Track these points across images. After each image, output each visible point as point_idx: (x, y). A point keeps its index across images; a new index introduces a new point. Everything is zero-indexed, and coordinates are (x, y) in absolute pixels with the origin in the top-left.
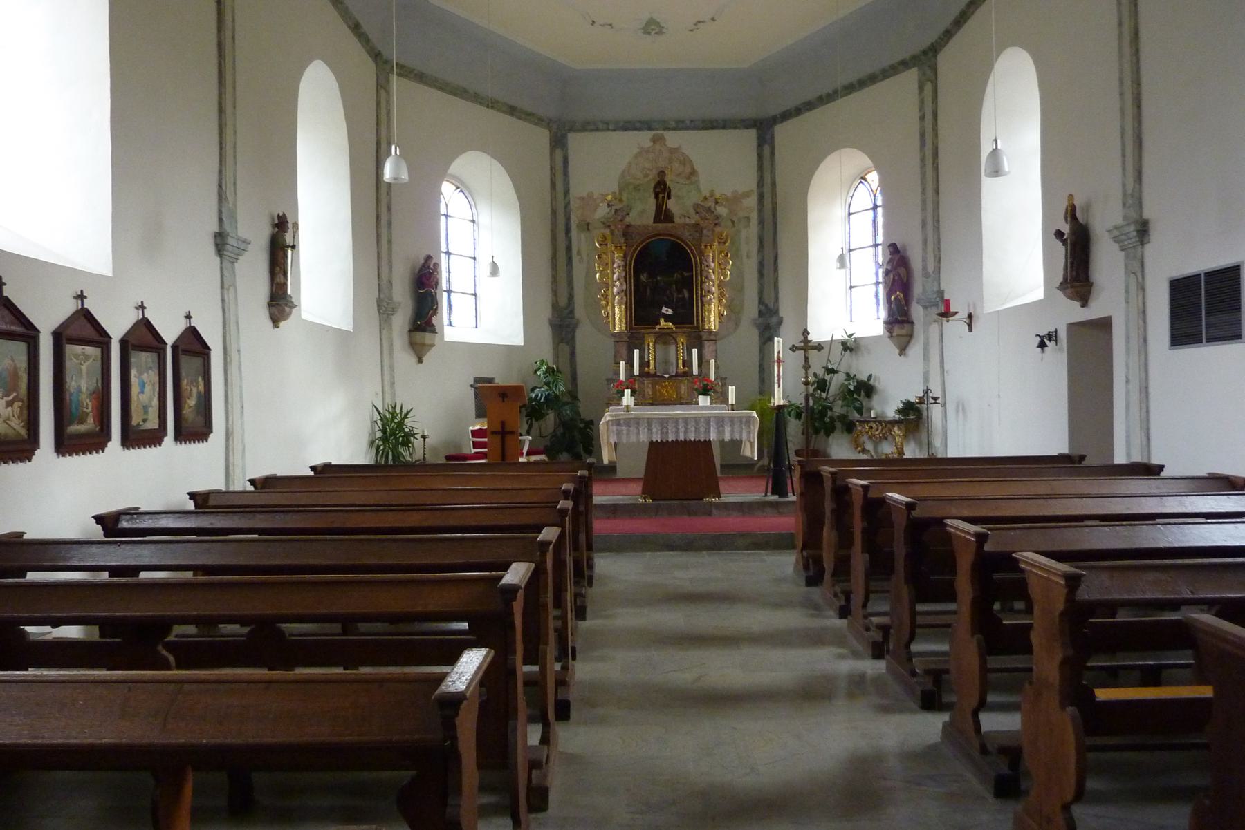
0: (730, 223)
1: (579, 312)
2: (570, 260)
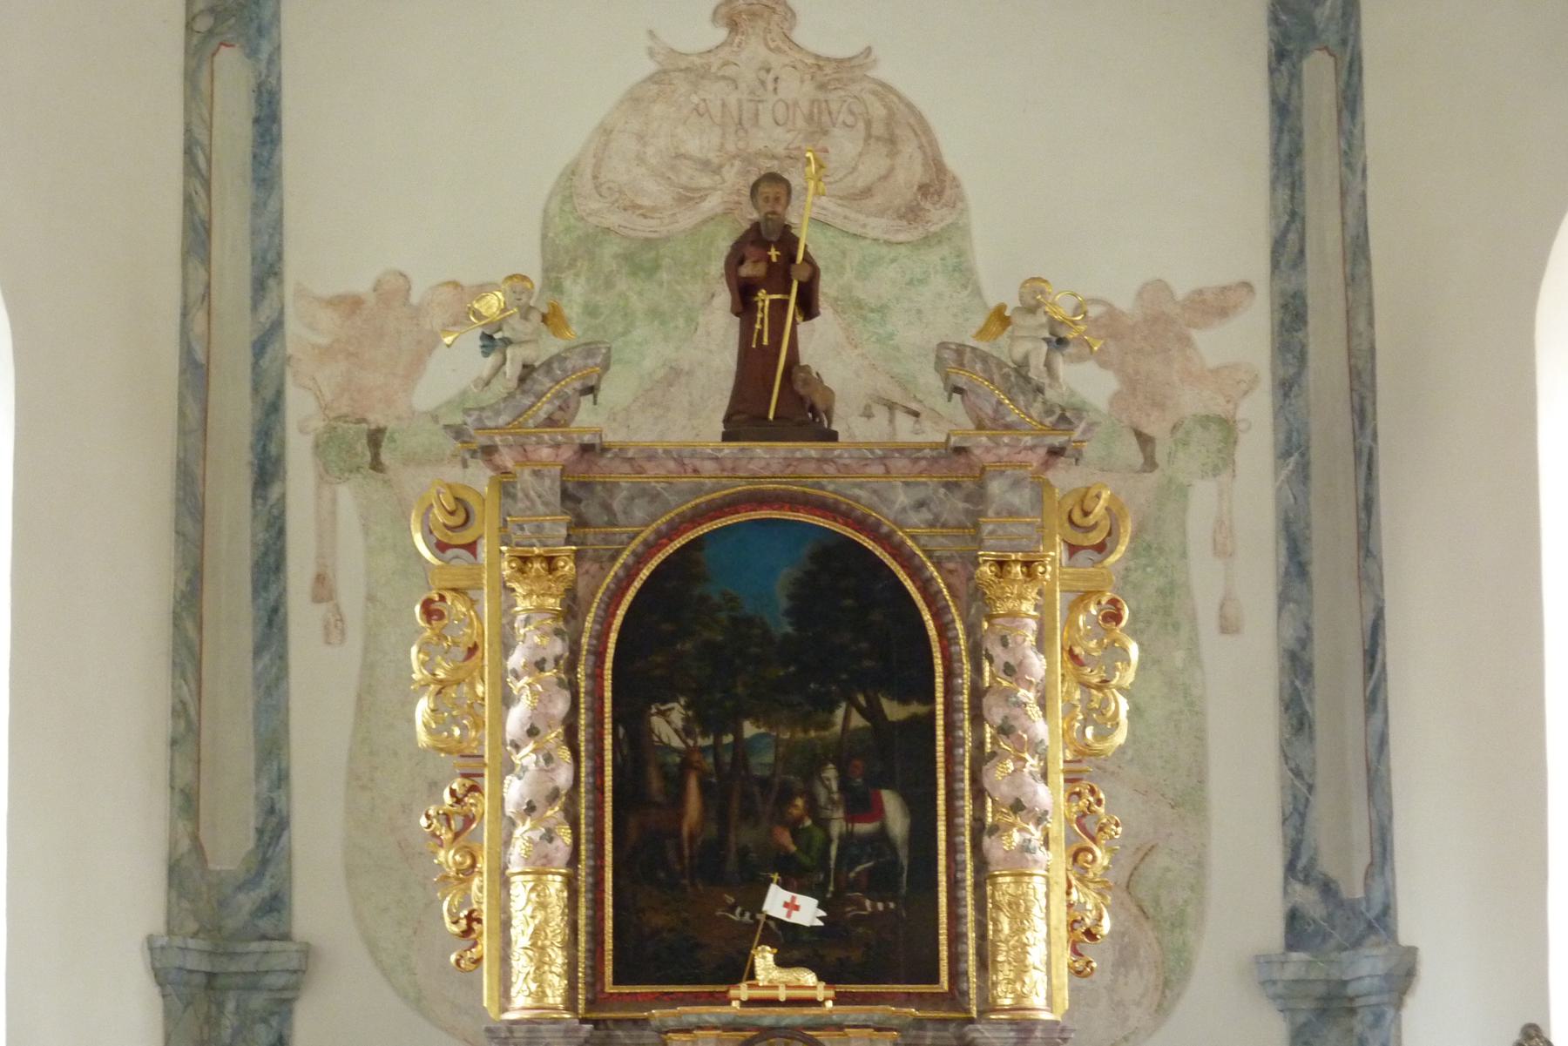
0: (1130, 451)
1: (319, 905)
2: (272, 624)
